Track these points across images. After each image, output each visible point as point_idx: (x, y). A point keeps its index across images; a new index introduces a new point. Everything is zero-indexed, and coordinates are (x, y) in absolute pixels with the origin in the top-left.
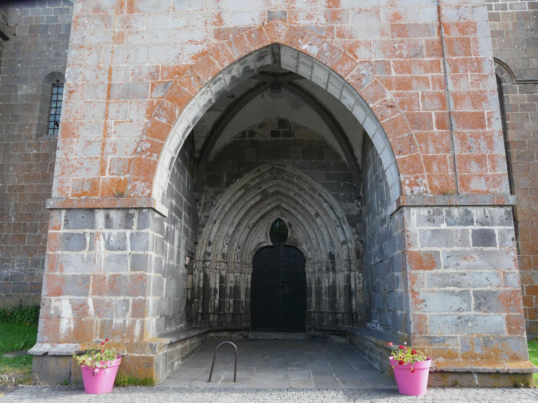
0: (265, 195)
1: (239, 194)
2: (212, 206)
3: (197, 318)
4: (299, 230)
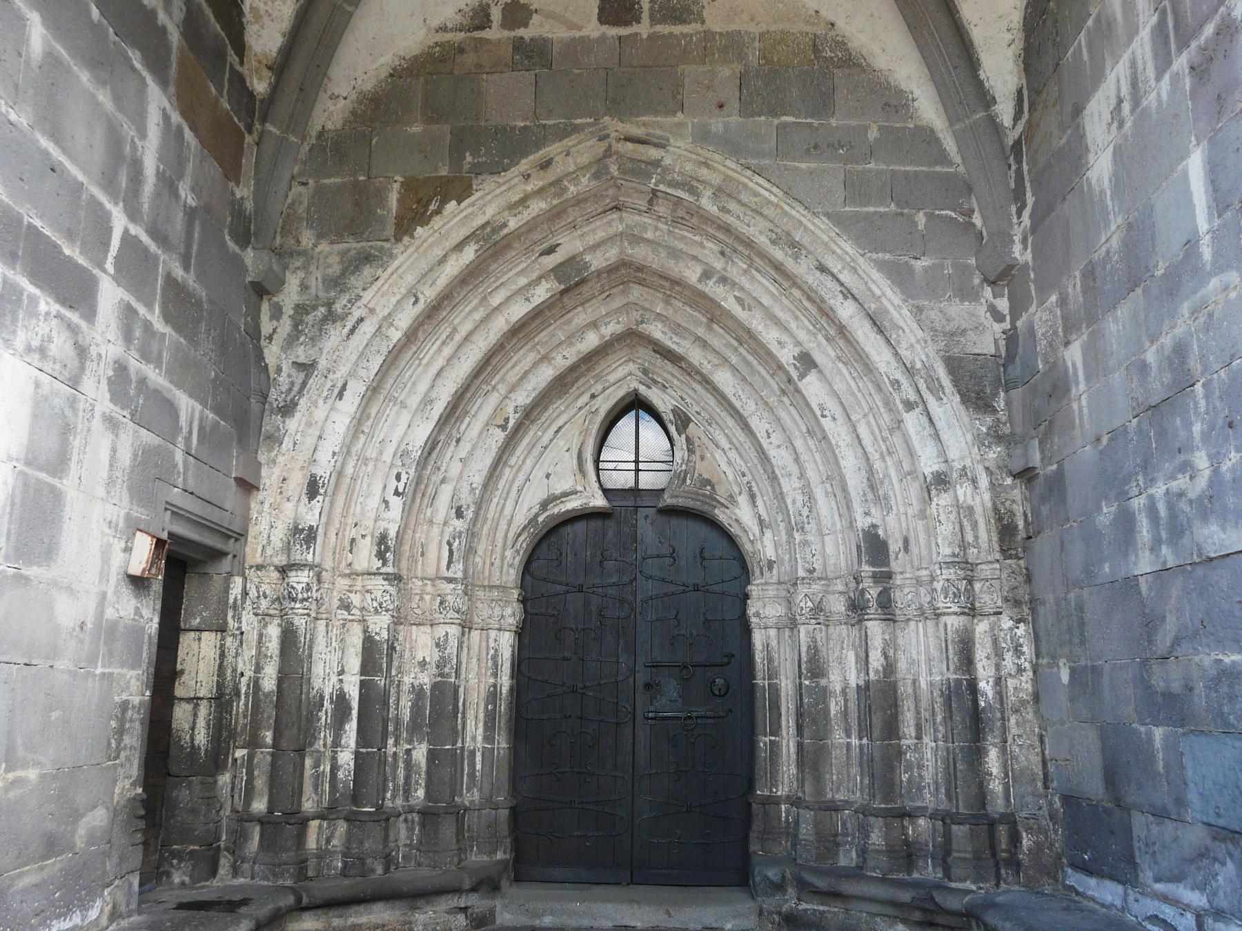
0: (573, 282)
1: (453, 267)
2: (331, 317)
3: (239, 837)
4: (724, 443)
